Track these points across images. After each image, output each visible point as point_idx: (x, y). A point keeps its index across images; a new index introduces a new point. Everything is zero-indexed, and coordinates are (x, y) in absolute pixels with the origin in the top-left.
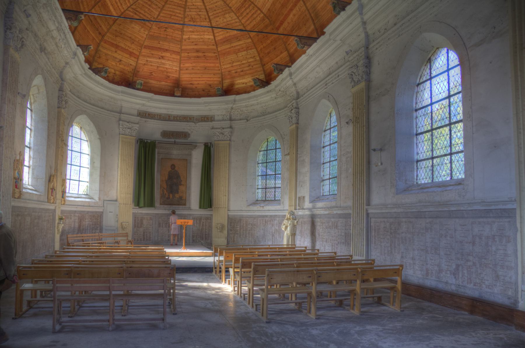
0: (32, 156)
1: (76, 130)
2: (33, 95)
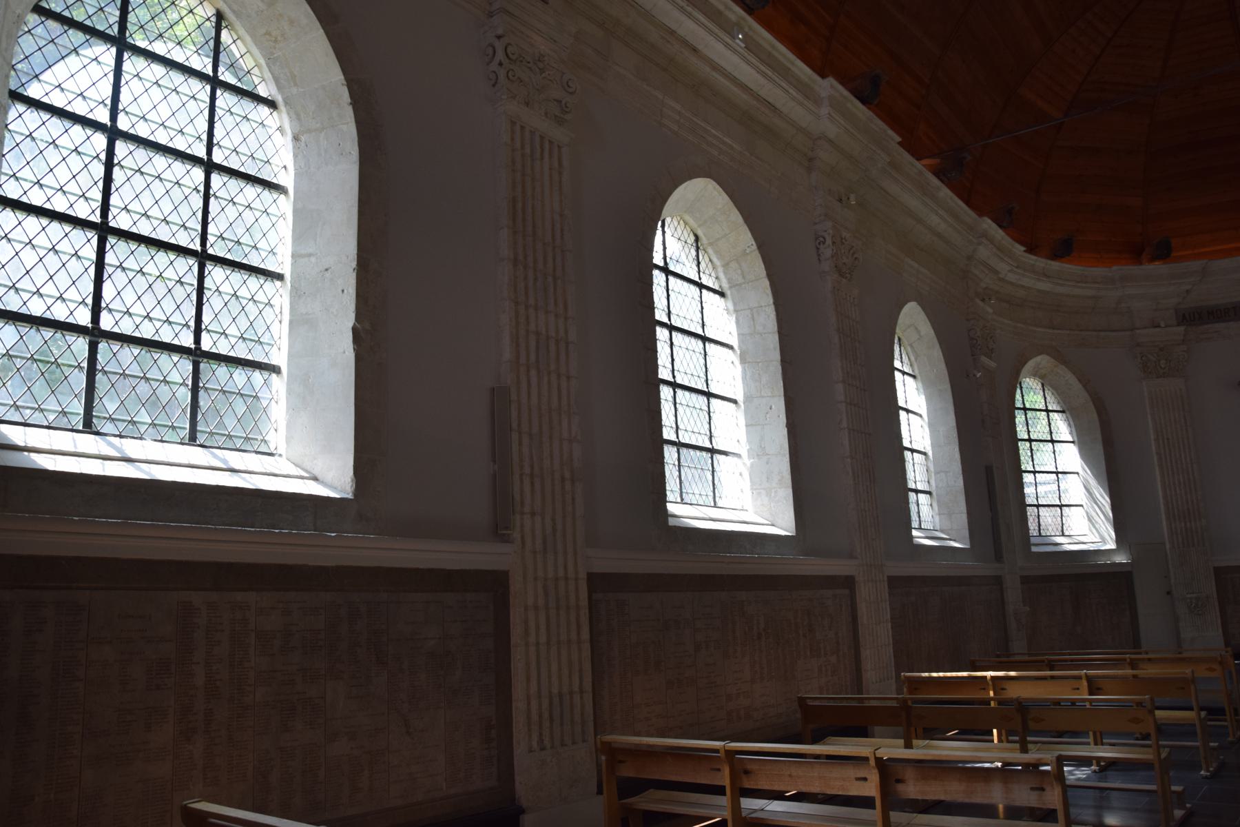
0: (932, 468)
1: (1032, 394)
2: (911, 346)
